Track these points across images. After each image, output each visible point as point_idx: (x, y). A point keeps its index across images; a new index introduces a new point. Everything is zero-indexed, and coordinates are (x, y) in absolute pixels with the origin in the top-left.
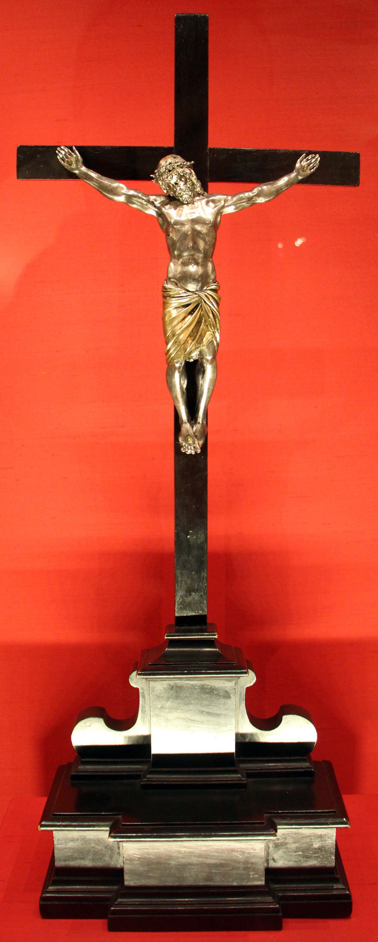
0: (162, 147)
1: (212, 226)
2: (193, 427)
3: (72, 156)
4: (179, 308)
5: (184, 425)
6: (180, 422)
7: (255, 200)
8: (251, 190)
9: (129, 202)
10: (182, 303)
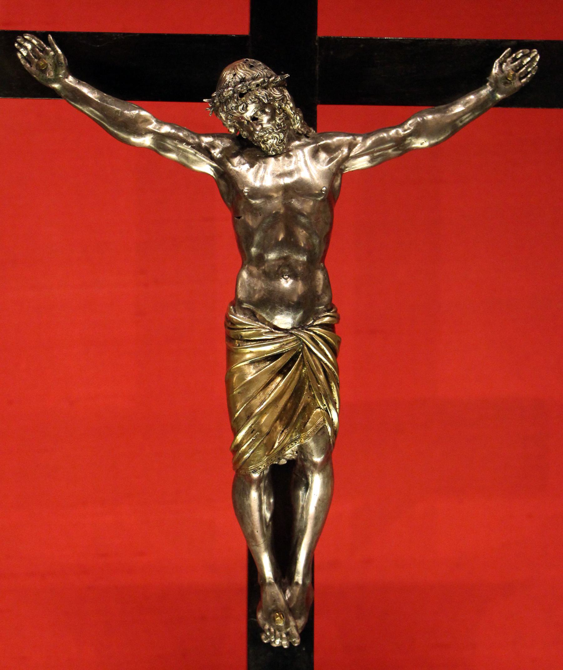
0: (226, 36)
1: (323, 200)
2: (284, 592)
3: (47, 53)
4: (259, 362)
5: (268, 589)
6: (260, 582)
7: (409, 144)
8: (401, 124)
9: (160, 148)
10: (264, 352)
